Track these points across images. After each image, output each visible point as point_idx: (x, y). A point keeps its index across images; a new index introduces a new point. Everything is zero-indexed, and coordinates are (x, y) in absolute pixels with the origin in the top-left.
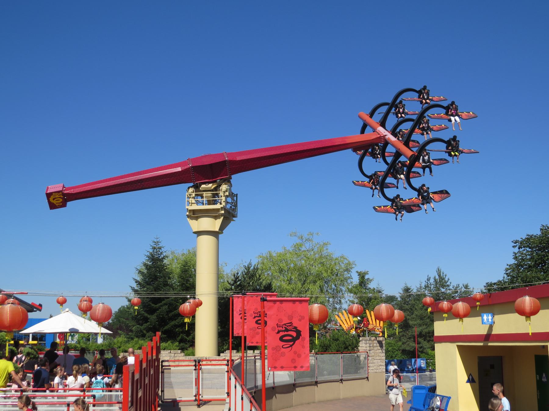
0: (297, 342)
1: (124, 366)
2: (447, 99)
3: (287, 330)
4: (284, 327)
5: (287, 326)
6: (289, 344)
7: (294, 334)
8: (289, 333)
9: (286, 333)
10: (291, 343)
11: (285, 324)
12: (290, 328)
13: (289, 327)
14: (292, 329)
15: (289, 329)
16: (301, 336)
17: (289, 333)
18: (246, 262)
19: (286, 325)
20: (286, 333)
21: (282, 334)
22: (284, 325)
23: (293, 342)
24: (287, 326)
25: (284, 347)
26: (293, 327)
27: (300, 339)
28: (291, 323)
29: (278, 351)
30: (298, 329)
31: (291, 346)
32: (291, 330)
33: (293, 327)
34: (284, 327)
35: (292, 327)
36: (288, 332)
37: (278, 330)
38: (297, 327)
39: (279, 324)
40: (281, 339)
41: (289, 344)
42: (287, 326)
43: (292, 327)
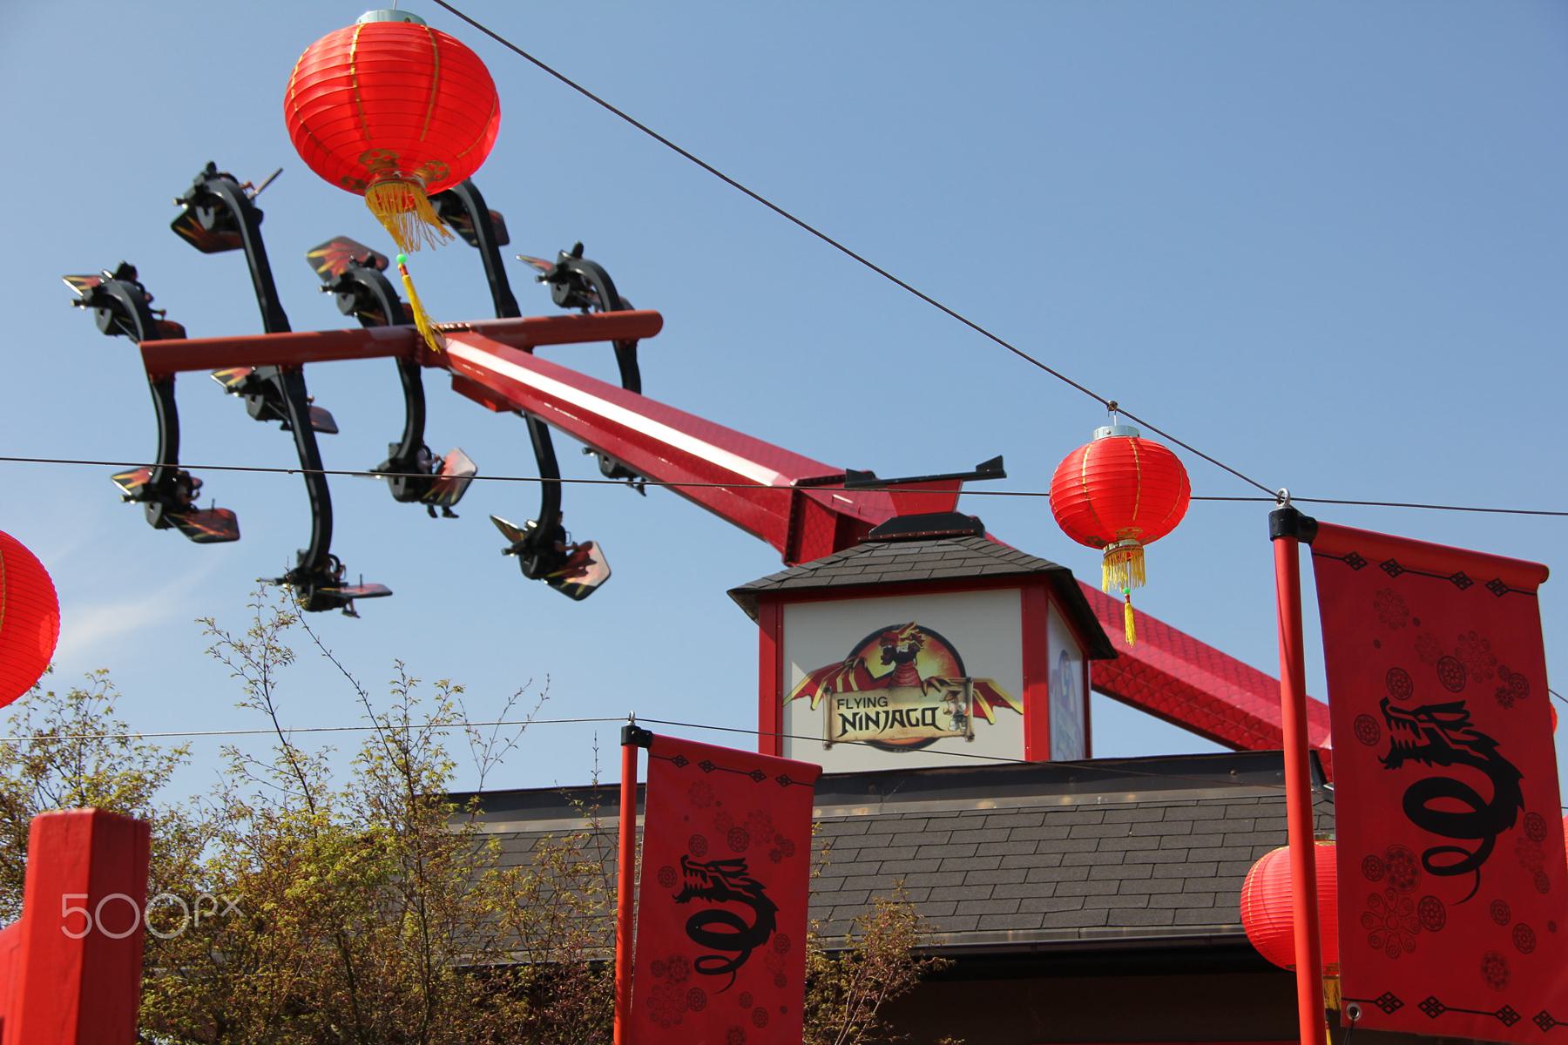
0: (1506, 840)
1: (549, 275)
2: (391, 588)
3: (719, 892)
4: (711, 877)
5: (721, 872)
6: (724, 958)
7: (748, 915)
8: (732, 907)
9: (715, 905)
10: (734, 955)
11: (715, 864)
12: (1454, 741)
13: (732, 881)
14: (740, 890)
15: (1454, 747)
16: (775, 931)
17: (732, 907)
18: (103, 725)
19: (1432, 719)
20: (715, 905)
21: (699, 905)
22: (711, 868)
23: (739, 953)
24: (721, 872)
25: (1434, 861)
26: (1472, 738)
27: (768, 943)
28: (739, 862)
29: (677, 981)
30: (767, 893)
31: (732, 967)
32: (1462, 758)
33: (1472, 738)
34: (711, 877)
35: (742, 883)
36: (1448, 764)
37: (685, 884)
38: (764, 888)
39: (1394, 702)
40: (694, 928)
41: (724, 958)
42: (726, 875)
43: (742, 883)
